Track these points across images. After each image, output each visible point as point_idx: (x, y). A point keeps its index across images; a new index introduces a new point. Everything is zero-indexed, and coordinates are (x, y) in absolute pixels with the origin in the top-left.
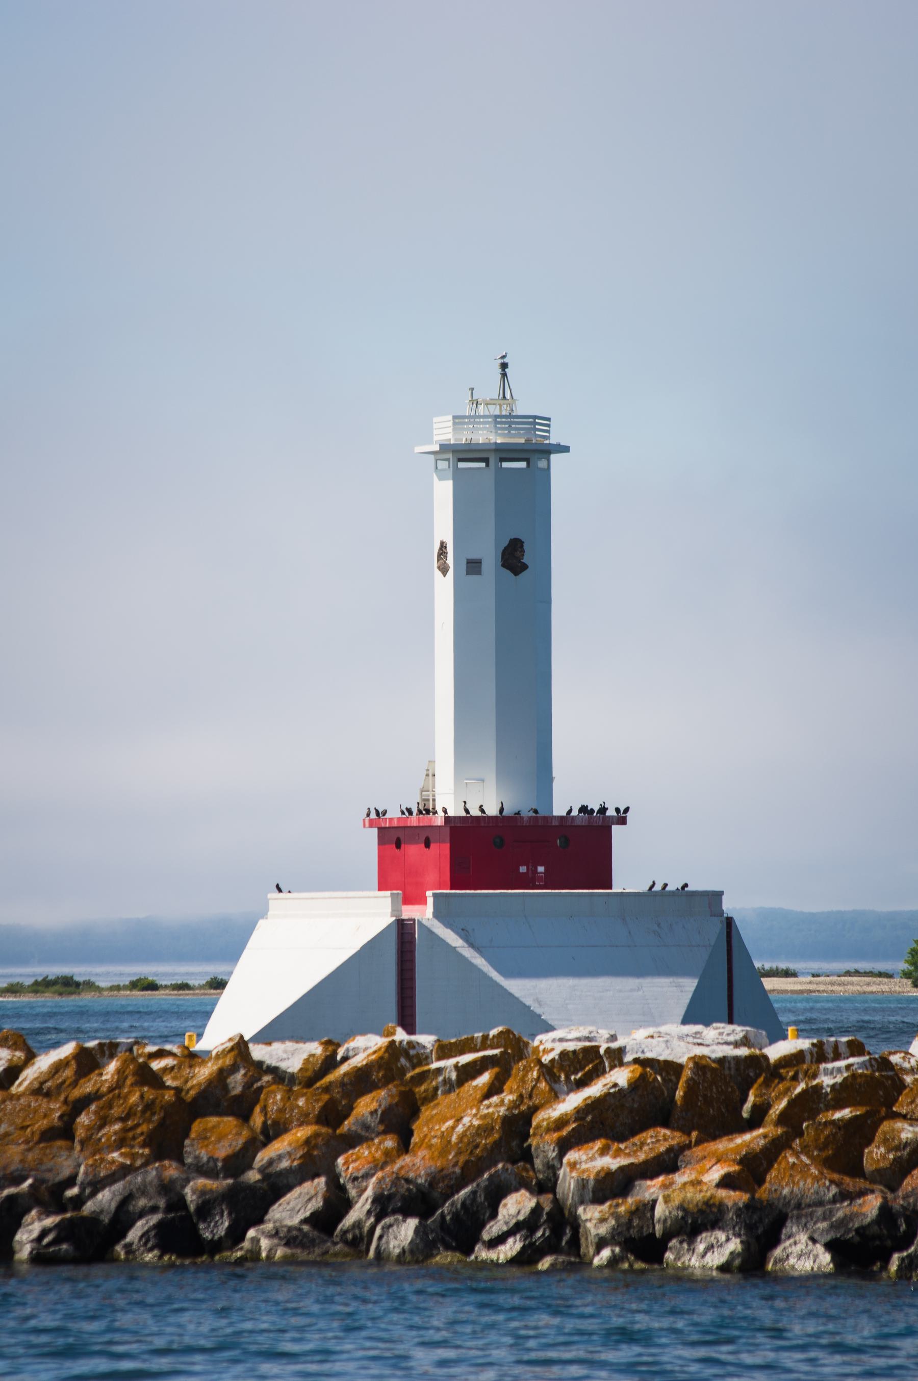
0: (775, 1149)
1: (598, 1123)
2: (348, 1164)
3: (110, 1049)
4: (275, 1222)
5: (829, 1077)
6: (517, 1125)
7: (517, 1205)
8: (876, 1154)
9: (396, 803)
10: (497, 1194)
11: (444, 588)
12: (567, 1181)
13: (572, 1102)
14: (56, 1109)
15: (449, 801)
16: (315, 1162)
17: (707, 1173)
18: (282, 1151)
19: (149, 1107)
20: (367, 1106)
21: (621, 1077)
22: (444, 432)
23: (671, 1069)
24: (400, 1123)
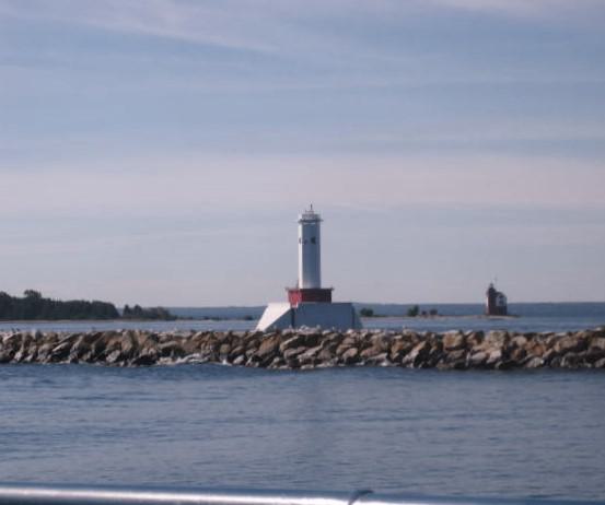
0: (320, 350)
1: (290, 346)
2: (248, 352)
3: (208, 333)
4: (593, 367)
5: (332, 337)
6: (277, 347)
7: (277, 360)
8: (338, 351)
9: (292, 286)
10: (272, 359)
11: (300, 246)
12: (285, 355)
13: (287, 342)
14: (197, 343)
15: (301, 286)
16: (242, 352)
17: (310, 353)
18: (238, 349)
19: (355, 338)
20: (252, 342)
21: (296, 338)
22: (300, 217)
23: (304, 336)
24: (258, 345)
